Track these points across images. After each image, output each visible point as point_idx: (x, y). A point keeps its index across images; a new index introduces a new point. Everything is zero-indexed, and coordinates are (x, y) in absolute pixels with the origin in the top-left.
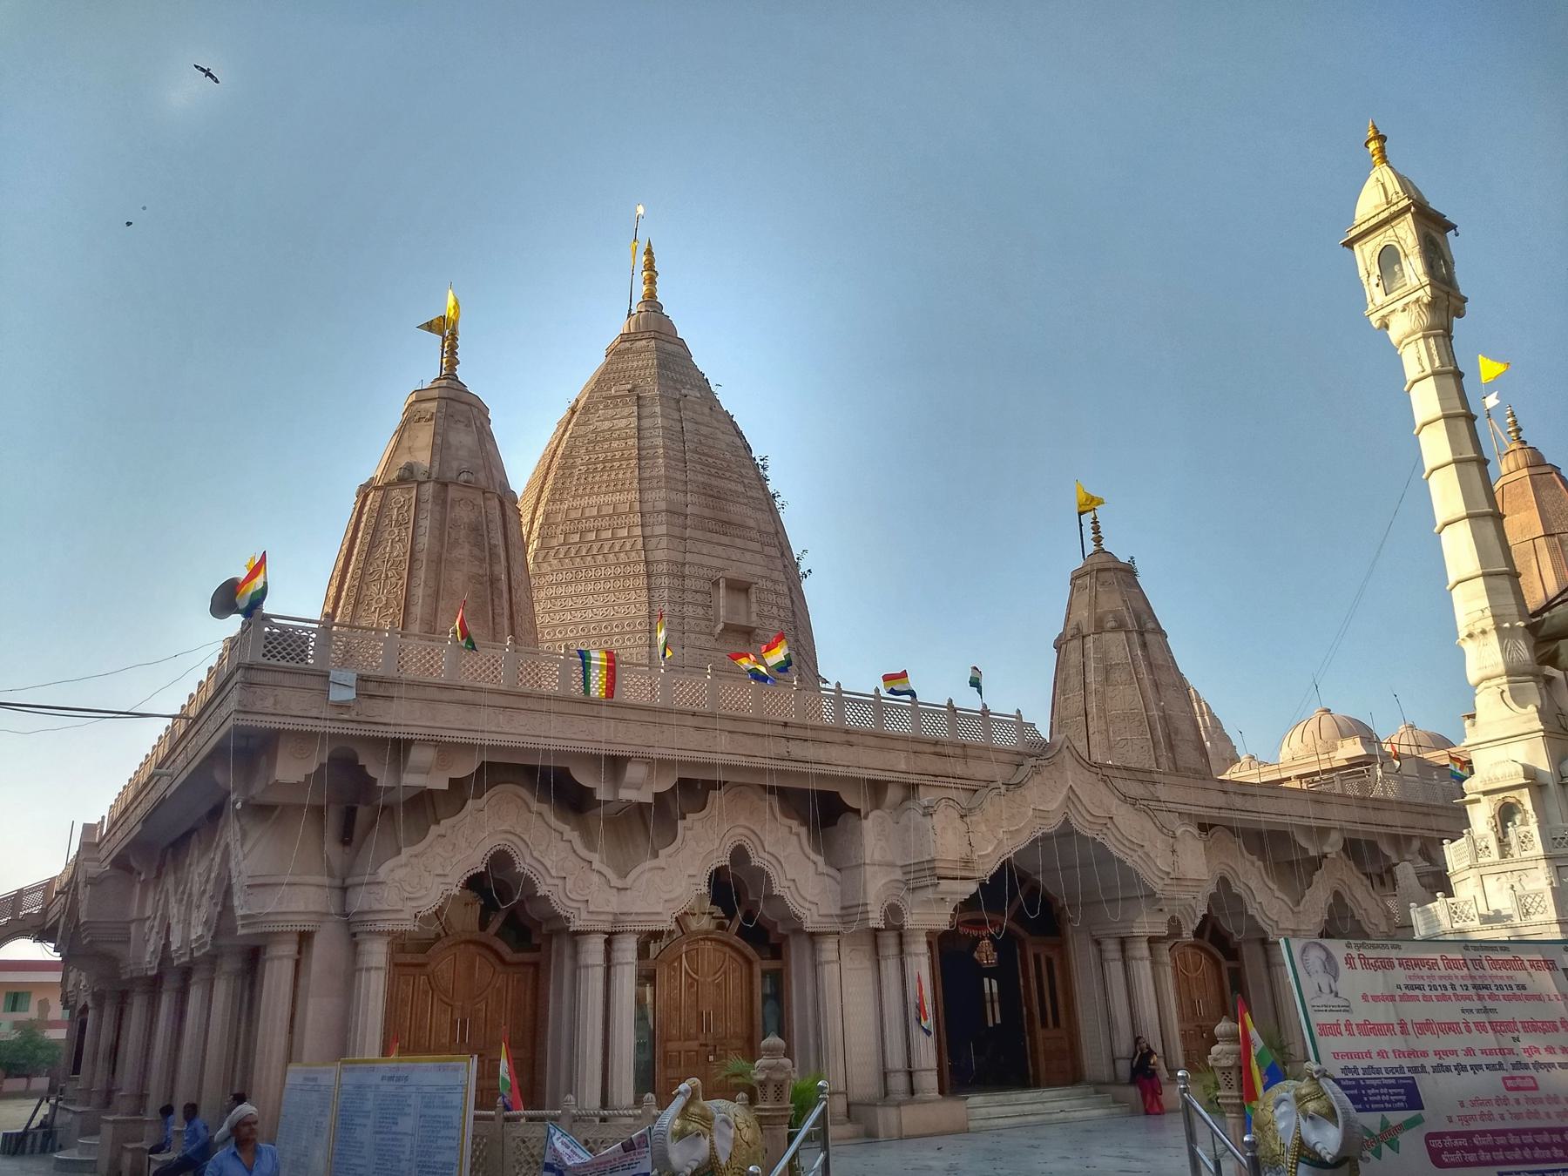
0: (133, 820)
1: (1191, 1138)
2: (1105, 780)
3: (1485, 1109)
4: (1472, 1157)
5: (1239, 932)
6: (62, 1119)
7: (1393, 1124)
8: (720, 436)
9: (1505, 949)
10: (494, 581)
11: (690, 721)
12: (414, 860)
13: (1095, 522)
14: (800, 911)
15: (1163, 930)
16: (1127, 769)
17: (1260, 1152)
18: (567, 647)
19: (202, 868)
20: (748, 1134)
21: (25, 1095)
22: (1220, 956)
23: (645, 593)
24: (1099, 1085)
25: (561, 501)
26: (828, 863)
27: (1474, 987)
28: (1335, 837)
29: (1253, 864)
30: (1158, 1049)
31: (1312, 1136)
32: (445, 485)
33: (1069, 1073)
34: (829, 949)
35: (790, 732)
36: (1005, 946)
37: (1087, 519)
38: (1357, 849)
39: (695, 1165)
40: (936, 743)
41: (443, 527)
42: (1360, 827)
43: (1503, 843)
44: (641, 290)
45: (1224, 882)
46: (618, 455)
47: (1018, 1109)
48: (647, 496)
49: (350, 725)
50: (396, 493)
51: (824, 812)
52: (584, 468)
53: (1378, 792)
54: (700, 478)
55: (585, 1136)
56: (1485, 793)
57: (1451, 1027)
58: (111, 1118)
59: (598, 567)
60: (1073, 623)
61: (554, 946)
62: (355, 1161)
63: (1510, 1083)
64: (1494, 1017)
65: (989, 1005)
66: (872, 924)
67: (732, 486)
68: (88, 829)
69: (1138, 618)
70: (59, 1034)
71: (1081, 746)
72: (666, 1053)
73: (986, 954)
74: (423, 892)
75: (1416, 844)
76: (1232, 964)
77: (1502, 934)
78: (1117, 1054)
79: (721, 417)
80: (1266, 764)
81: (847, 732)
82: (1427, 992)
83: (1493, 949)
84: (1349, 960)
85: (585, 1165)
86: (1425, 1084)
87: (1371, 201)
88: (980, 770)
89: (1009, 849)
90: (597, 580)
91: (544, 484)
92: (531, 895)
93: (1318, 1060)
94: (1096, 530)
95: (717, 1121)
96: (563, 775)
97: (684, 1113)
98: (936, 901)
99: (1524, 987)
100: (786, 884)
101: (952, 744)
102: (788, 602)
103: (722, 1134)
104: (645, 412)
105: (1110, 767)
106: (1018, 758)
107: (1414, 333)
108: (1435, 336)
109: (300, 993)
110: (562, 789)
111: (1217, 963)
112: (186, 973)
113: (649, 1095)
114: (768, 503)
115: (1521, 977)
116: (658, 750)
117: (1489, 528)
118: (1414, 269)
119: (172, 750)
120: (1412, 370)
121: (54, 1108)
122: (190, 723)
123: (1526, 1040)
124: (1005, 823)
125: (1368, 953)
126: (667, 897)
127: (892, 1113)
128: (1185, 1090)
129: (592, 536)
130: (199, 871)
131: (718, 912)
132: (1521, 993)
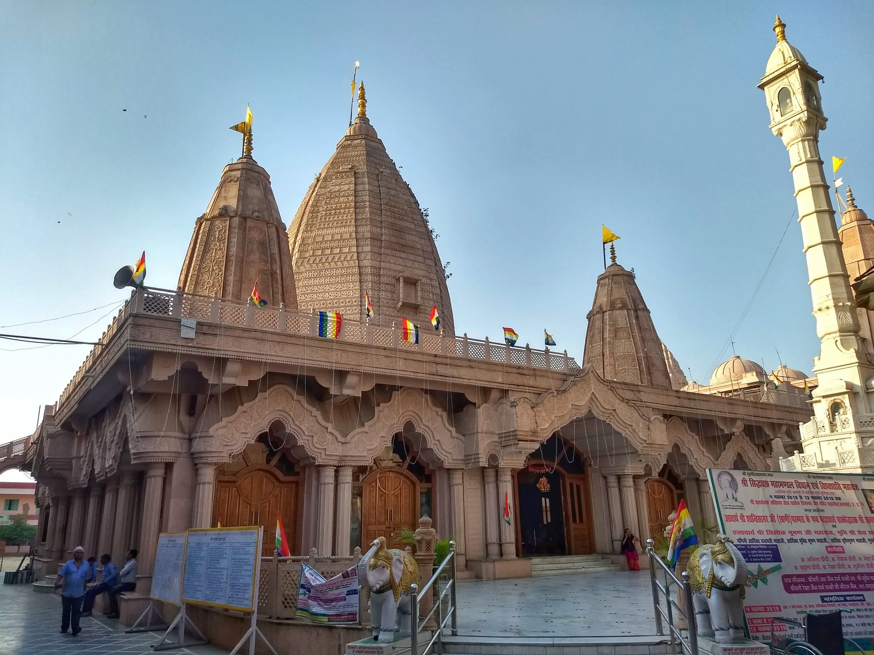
0: (73, 402)
2: (612, 389)
3: (815, 563)
4: (807, 588)
5: (684, 474)
6: (37, 566)
7: (765, 569)
8: (401, 196)
9: (830, 478)
10: (273, 273)
11: (383, 352)
12: (229, 424)
13: (612, 248)
14: (442, 457)
15: (642, 472)
16: (624, 383)
17: (691, 582)
18: (314, 310)
19: (112, 428)
21: (16, 555)
22: (673, 488)
23: (358, 284)
24: (604, 555)
25: (311, 231)
27: (812, 497)
28: (739, 423)
29: (693, 437)
30: (637, 535)
31: (719, 573)
32: (245, 219)
33: (588, 548)
34: (457, 478)
35: (437, 360)
36: (554, 478)
37: (608, 246)
38: (752, 431)
39: (381, 583)
40: (519, 368)
41: (244, 243)
42: (753, 419)
43: (832, 424)
45: (676, 447)
47: (559, 565)
48: (360, 229)
49: (193, 349)
50: (217, 222)
51: (457, 405)
53: (764, 399)
54: (390, 220)
55: (323, 569)
56: (824, 397)
57: (798, 519)
59: (332, 269)
60: (598, 305)
61: (307, 473)
62: (196, 583)
63: (830, 549)
64: (822, 514)
66: (481, 464)
67: (408, 225)
68: (48, 408)
69: (634, 302)
70: (34, 523)
71: (600, 372)
72: (367, 531)
73: (544, 485)
74: (234, 442)
75: (784, 428)
76: (679, 492)
77: (827, 470)
78: (614, 538)
80: (703, 386)
81: (470, 360)
82: (787, 500)
83: (824, 478)
84: (744, 482)
85: (322, 585)
86: (783, 549)
87: (775, 62)
88: (542, 383)
89: (558, 426)
90: (331, 276)
91: (301, 221)
92: (295, 446)
93: (724, 533)
94: (613, 252)
95: (394, 559)
98: (516, 452)
99: (839, 499)
101: (528, 368)
102: (438, 291)
103: (396, 567)
104: (359, 181)
105: (615, 382)
106: (564, 377)
107: (797, 138)
108: (808, 140)
109: (166, 495)
110: (311, 388)
111: (671, 491)
112: (103, 486)
113: (358, 548)
114: (428, 235)
115: (838, 493)
116: (364, 368)
117: (834, 249)
118: (798, 101)
119: (94, 363)
120: (794, 160)
121: (32, 560)
122: (104, 347)
123: (841, 526)
125: (755, 478)
126: (368, 448)
127: (490, 565)
128: (651, 550)
130: (110, 430)
131: (397, 458)
132: (837, 501)
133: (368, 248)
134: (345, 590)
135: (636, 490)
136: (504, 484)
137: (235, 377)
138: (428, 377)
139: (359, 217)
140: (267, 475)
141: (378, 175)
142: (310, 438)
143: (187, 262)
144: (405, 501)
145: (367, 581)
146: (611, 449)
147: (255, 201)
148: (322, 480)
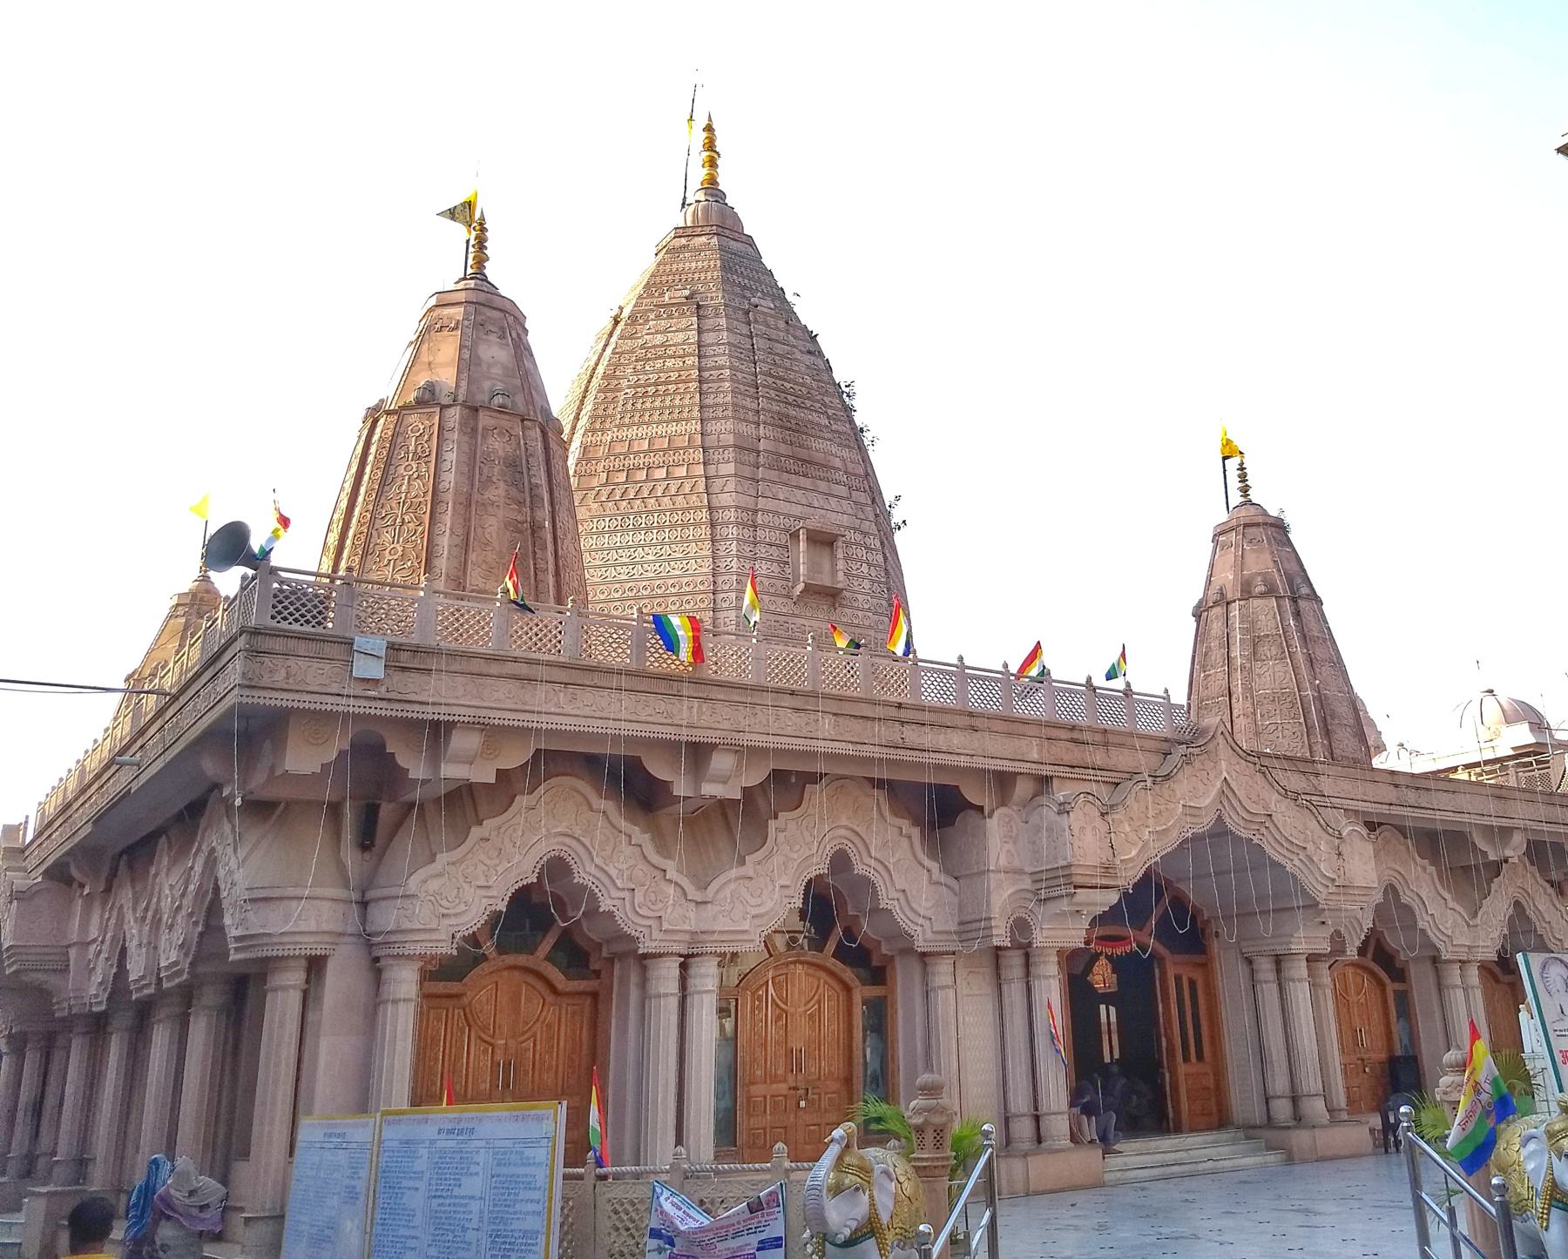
1: (1416, 1184)
2: (1264, 771)
8: (798, 355)
10: (535, 528)
11: (788, 701)
13: (1242, 468)
15: (1325, 947)
18: (640, 610)
20: (908, 1187)
22: (1387, 980)
23: (708, 545)
25: (603, 431)
26: (945, 870)
28: (1518, 839)
29: (1424, 869)
33: (1218, 1118)
34: (942, 972)
35: (903, 714)
37: (1232, 464)
39: (854, 1225)
40: (1073, 728)
41: (472, 463)
42: (1546, 827)
44: (698, 174)
45: (1391, 890)
46: (674, 376)
48: (712, 427)
49: (380, 704)
50: (413, 419)
51: (941, 811)
52: (631, 392)
55: (703, 1194)
58: (43, 1190)
61: (616, 972)
62: (402, 1232)
65: (1105, 1038)
66: (996, 942)
67: (814, 417)
72: (749, 1099)
74: (462, 908)
76: (1398, 986)
79: (799, 333)
81: (971, 715)
85: (702, 1230)
88: (1123, 759)
89: (1157, 850)
90: (648, 529)
91: (580, 409)
92: (593, 912)
94: (1243, 478)
95: (876, 1173)
96: (635, 767)
97: (839, 1163)
98: (1071, 913)
100: (896, 895)
101: (1090, 729)
102: (880, 558)
104: (708, 324)
105: (1268, 756)
106: (1165, 746)
110: (632, 784)
111: (1381, 985)
112: (144, 1013)
114: (855, 438)
116: (747, 736)
124: (1151, 822)
126: (754, 911)
127: (1017, 1166)
129: (642, 475)
130: (171, 884)
133: (730, 468)
134: (754, 1240)
135: (1314, 986)
136: (1044, 983)
137: (464, 763)
138: (877, 752)
139: (709, 401)
140: (531, 979)
141: (747, 313)
142: (626, 894)
143: (344, 504)
144: (830, 1026)
145: (822, 1220)
146: (1261, 899)
147: (496, 371)
148: (653, 988)
